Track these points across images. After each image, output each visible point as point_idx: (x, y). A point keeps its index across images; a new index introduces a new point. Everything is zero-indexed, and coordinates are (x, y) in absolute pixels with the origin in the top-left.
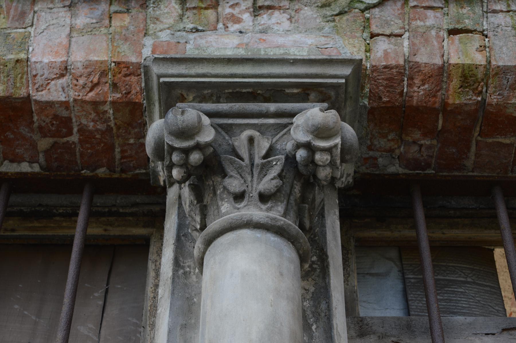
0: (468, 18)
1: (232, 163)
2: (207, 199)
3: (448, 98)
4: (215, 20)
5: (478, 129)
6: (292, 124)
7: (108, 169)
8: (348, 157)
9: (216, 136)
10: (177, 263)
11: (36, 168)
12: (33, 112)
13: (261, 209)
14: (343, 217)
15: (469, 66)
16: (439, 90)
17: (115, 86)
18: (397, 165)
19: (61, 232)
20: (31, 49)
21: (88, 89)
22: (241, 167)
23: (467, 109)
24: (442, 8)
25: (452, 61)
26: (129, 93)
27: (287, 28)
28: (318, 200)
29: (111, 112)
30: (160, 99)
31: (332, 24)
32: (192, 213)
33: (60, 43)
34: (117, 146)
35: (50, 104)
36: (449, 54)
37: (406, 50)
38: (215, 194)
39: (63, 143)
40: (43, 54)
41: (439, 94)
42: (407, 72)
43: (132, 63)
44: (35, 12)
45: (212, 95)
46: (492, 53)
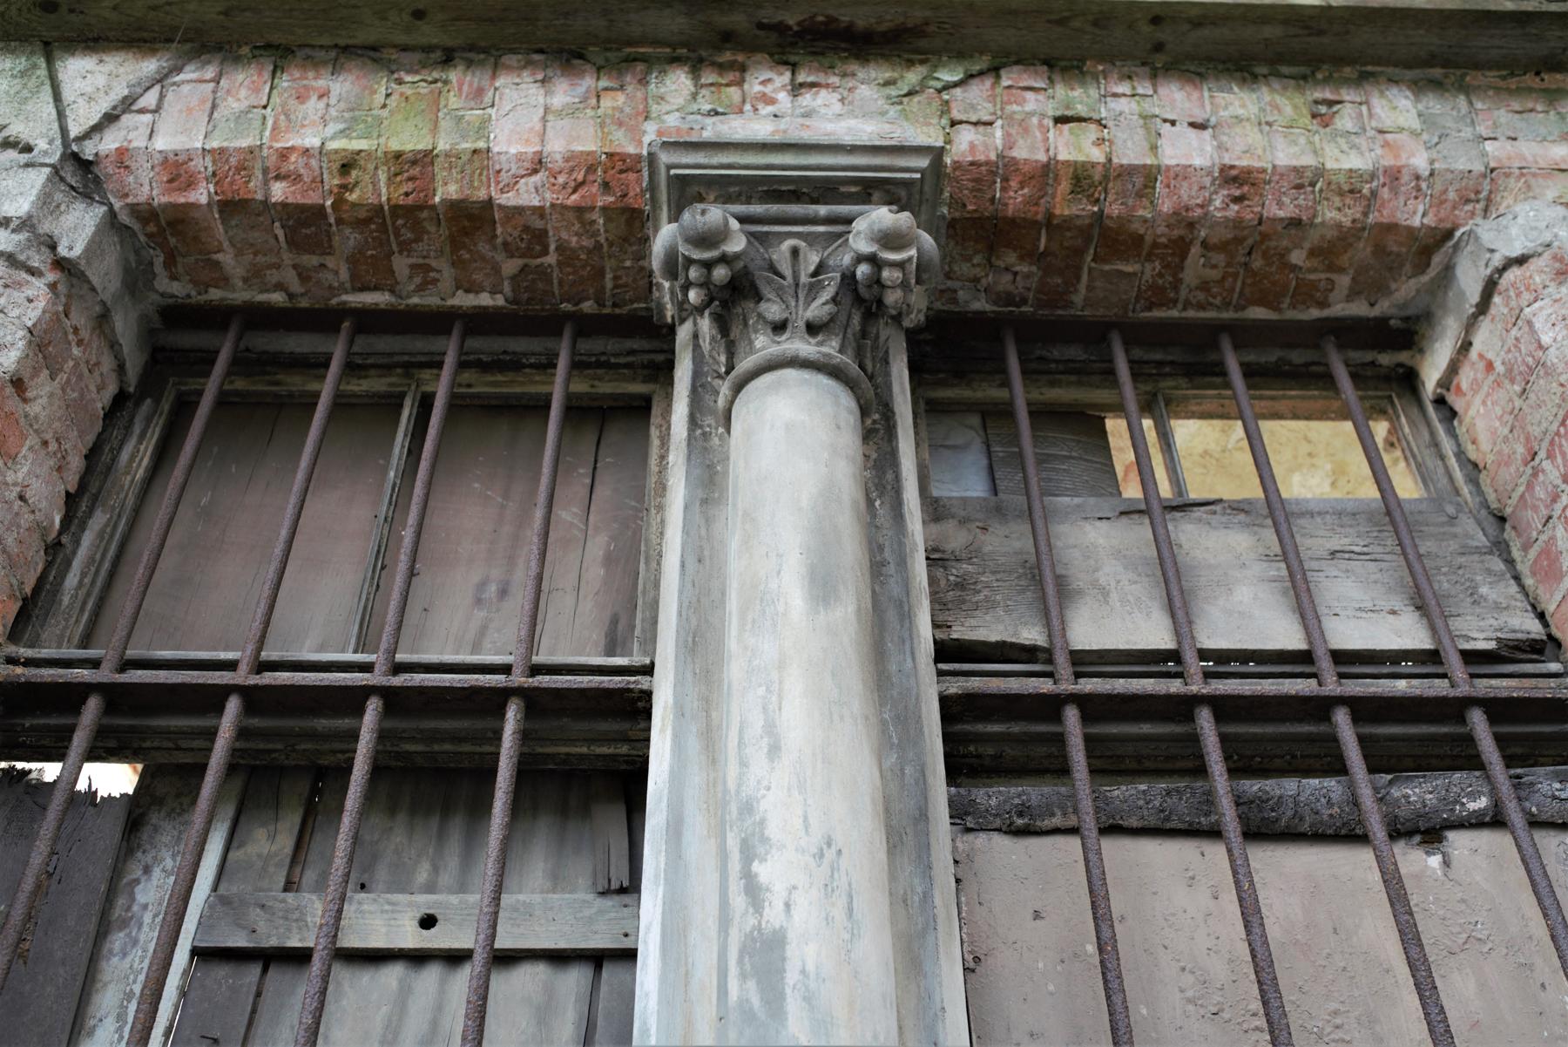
0: (1081, 103)
1: (769, 282)
2: (735, 332)
3: (1054, 207)
4: (740, 99)
5: (1092, 251)
6: (849, 232)
7: (597, 302)
8: (925, 276)
9: (746, 247)
10: (693, 421)
11: (500, 301)
12: (495, 222)
13: (809, 343)
14: (914, 369)
15: (1084, 164)
16: (1042, 197)
17: (606, 186)
18: (984, 301)
19: (532, 389)
20: (492, 136)
21: (570, 190)
22: (781, 288)
23: (1079, 222)
24: (1045, 90)
25: (1061, 157)
26: (625, 196)
27: (838, 112)
28: (882, 338)
29: (601, 221)
30: (669, 200)
31: (899, 107)
32: (715, 354)
33: (532, 129)
34: (608, 270)
35: (519, 210)
36: (1056, 148)
37: (999, 142)
38: (746, 324)
39: (537, 267)
40: (509, 142)
41: (1042, 201)
42: (1000, 171)
43: (630, 155)
44: (496, 89)
45: (740, 195)
46: (1114, 148)
